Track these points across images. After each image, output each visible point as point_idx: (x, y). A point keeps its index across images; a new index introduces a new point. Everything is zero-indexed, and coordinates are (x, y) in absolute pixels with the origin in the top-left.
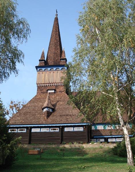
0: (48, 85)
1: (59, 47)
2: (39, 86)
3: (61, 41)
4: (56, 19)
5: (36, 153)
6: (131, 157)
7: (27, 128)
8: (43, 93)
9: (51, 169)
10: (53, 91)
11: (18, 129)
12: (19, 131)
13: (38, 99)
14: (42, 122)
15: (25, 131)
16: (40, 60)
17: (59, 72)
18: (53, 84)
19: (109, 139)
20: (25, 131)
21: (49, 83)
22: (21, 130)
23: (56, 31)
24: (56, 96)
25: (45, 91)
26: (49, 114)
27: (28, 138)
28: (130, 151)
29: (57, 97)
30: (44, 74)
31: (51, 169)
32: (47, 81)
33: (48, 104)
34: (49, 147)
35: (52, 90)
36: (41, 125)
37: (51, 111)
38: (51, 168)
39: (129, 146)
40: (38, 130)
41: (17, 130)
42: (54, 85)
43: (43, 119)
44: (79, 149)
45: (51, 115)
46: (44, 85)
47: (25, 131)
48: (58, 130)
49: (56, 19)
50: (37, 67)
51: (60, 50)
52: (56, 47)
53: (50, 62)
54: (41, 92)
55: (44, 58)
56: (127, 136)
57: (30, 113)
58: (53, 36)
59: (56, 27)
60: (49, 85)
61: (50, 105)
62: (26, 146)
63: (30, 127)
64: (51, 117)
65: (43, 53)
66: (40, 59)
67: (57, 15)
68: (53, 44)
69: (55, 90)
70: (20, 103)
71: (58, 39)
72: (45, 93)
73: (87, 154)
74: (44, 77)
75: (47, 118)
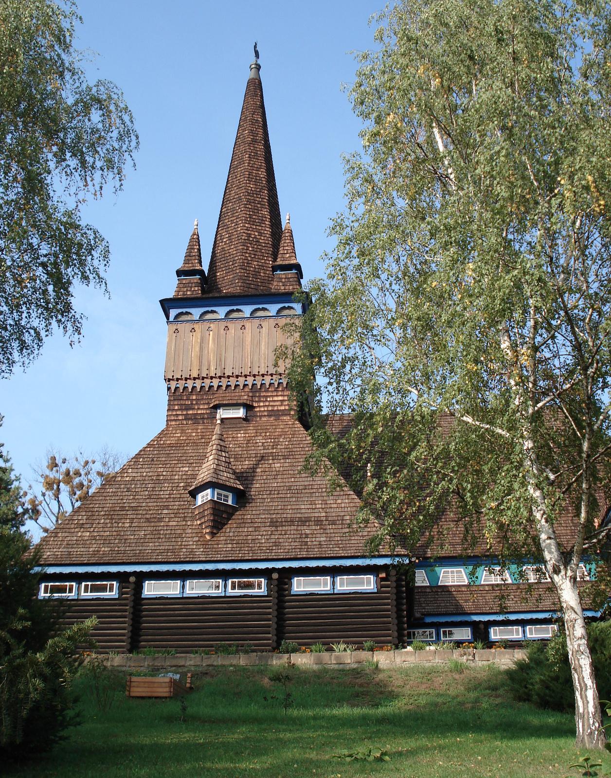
1: (266, 212)
2: (177, 388)
4: (255, 88)
6: (591, 709)
7: (121, 577)
8: (195, 419)
10: (240, 413)
16: (179, 273)
17: (265, 324)
18: (241, 381)
19: (492, 630)
20: (114, 594)
21: (220, 377)
22: (95, 589)
23: (254, 141)
28: (589, 682)
29: (260, 440)
30: (198, 335)
32: (212, 368)
35: (236, 405)
37: (230, 503)
39: (582, 662)
40: (171, 589)
41: (79, 589)
42: (245, 385)
43: (193, 536)
44: (356, 673)
45: (229, 519)
46: (198, 384)
48: (260, 588)
49: (255, 88)
51: (272, 226)
53: (228, 282)
55: (200, 263)
56: (573, 616)
57: (134, 509)
58: (241, 162)
59: (253, 122)
60: (219, 387)
61: (226, 477)
63: (135, 573)
64: (230, 529)
65: (195, 241)
66: (179, 264)
67: (258, 67)
69: (249, 407)
70: (90, 464)
71: (263, 174)
73: (392, 696)
74: (198, 349)
75: (213, 534)
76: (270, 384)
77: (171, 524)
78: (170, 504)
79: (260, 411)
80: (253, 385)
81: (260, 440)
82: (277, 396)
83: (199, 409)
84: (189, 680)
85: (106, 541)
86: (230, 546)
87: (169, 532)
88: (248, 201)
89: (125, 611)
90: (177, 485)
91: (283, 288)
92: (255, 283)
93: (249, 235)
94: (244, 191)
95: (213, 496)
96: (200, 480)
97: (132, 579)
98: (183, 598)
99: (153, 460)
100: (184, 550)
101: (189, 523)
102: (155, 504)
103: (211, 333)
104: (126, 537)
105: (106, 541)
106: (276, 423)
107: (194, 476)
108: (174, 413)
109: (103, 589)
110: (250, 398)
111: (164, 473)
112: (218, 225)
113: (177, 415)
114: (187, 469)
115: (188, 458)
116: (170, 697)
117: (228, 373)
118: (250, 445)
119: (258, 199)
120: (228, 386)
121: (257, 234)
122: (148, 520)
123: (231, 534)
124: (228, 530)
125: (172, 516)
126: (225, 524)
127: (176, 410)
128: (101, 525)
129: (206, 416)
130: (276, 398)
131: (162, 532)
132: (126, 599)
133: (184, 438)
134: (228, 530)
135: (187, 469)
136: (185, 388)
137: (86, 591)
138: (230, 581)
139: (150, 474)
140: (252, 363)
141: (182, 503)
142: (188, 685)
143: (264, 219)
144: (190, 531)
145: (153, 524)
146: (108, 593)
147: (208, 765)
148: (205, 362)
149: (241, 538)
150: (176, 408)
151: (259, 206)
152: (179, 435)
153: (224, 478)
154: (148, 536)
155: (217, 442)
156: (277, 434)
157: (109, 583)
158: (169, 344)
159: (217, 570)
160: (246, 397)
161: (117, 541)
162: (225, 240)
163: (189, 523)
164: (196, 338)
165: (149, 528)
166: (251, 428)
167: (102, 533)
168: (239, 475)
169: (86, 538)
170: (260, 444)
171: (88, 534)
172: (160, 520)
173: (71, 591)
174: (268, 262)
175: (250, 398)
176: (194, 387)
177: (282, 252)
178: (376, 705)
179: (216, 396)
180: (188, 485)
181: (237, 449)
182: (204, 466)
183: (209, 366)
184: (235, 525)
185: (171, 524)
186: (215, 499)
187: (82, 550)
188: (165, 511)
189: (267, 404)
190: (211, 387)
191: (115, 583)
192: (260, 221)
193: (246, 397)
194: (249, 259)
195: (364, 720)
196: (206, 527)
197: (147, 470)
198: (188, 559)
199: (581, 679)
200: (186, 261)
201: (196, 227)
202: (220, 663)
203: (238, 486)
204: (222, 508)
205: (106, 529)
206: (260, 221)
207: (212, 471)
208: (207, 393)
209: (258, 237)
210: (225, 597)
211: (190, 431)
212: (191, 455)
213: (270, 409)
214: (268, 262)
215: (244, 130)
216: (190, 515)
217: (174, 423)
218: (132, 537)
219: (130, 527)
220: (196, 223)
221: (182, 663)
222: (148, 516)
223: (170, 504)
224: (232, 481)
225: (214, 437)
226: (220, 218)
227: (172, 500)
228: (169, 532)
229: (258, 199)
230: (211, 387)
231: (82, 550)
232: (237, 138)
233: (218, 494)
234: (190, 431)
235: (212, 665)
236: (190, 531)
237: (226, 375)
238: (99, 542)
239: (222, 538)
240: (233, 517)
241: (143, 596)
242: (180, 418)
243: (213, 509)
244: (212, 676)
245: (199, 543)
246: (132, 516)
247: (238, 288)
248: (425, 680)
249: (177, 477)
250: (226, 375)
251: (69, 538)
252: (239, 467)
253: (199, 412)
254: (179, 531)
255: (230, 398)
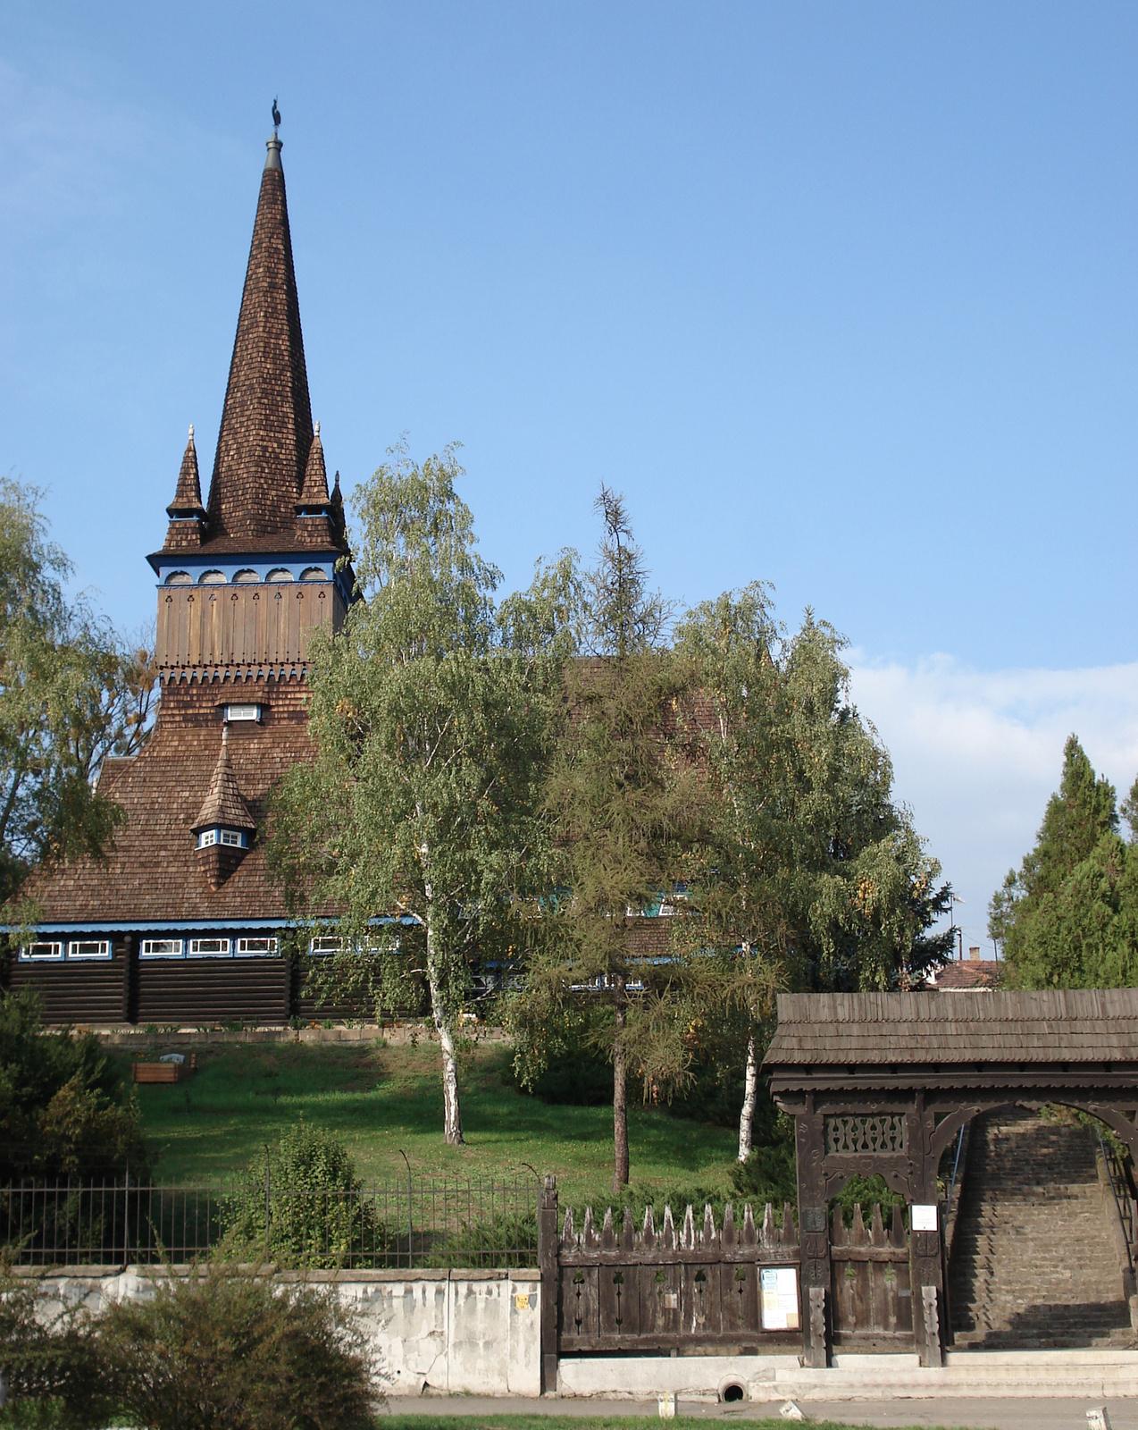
0: (221, 673)
1: (287, 409)
2: (172, 679)
3: (306, 387)
4: (274, 184)
5: (169, 1076)
6: (453, 1119)
7: (116, 937)
8: (197, 721)
9: (216, 1155)
10: (253, 714)
11: (66, 944)
12: (74, 952)
13: (166, 759)
14: (195, 907)
15: (105, 953)
16: (171, 512)
17: (284, 593)
18: (255, 670)
20: (107, 955)
21: (227, 666)
22: (84, 949)
23: (273, 286)
24: (268, 741)
25: (205, 709)
26: (227, 862)
27: (121, 974)
28: (453, 1100)
29: (277, 753)
30: (197, 604)
31: (216, 1155)
32: (217, 653)
33: (222, 809)
34: (228, 1043)
35: (249, 704)
36: (190, 926)
37: (239, 845)
38: (217, 1151)
39: (450, 1088)
40: (175, 950)
41: (66, 950)
42: (259, 677)
43: (196, 886)
44: (362, 1051)
45: (238, 864)
46: (199, 674)
47: (107, 955)
49: (274, 184)
50: (156, 561)
51: (296, 432)
52: (274, 408)
53: (239, 534)
54: (186, 719)
55: (199, 496)
56: (447, 1057)
58: (254, 324)
59: (272, 251)
60: (226, 678)
62: (110, 1033)
63: (130, 933)
64: (239, 879)
65: (191, 460)
67: (279, 146)
68: (251, 387)
69: (264, 707)
71: (284, 344)
72: (207, 720)
73: (384, 1076)
74: (197, 625)
75: (219, 885)
76: (292, 676)
77: (170, 870)
78: (168, 843)
79: (278, 712)
80: (270, 676)
81: (277, 753)
82: (300, 692)
83: (201, 707)
84: (193, 1061)
85: (95, 892)
86: (239, 899)
87: (167, 881)
88: (264, 391)
89: (121, 974)
90: (175, 816)
91: (308, 540)
92: (273, 524)
93: (265, 449)
94: (257, 375)
95: (219, 840)
96: (204, 817)
97: (128, 939)
98: (186, 959)
99: (145, 781)
100: (186, 905)
101: (191, 869)
102: (150, 843)
103: (215, 602)
104: (117, 887)
105: (95, 892)
106: (298, 729)
107: (198, 806)
108: (170, 712)
109: (94, 949)
110: (266, 695)
111: (160, 800)
112: (222, 426)
113: (173, 715)
114: (187, 794)
115: (189, 778)
116: (175, 1083)
117: (238, 660)
118: (264, 760)
119: (277, 388)
120: (237, 678)
121: (275, 445)
122: (143, 865)
123: (240, 884)
124: (237, 880)
125: (171, 859)
126: (233, 872)
127: (172, 709)
128: (86, 871)
129: (210, 717)
130: (298, 695)
131: (160, 881)
132: (121, 960)
133: (184, 748)
134: (237, 880)
135: (187, 794)
136: (183, 679)
137: (74, 952)
138: (239, 940)
139: (142, 801)
140: (268, 647)
141: (183, 842)
142: (193, 1066)
143: (286, 420)
144: (192, 880)
145: (148, 870)
146: (100, 954)
147: (202, 1155)
148: (208, 644)
149: (252, 889)
150: (172, 705)
151: (279, 399)
152: (176, 743)
153: (231, 817)
154: (144, 887)
155: (222, 770)
156: (298, 745)
157: (100, 943)
158: (160, 617)
159: (225, 929)
160: (260, 694)
161: (107, 892)
162: (232, 453)
163: (191, 869)
164: (194, 610)
165: (145, 876)
166: (267, 735)
167: (89, 882)
168: (251, 804)
169: (70, 888)
170: (278, 760)
171: (72, 882)
172: (157, 864)
173: (56, 952)
174: (290, 489)
175: (266, 695)
176: (194, 678)
177: (308, 484)
178: (372, 1088)
179: (222, 691)
180: (190, 818)
181: (249, 767)
182: (208, 799)
183: (213, 649)
184: (245, 873)
185: (170, 870)
186: (222, 843)
187: (67, 903)
188: (163, 853)
189: (287, 702)
190: (216, 678)
191: (107, 942)
192: (280, 424)
193: (260, 694)
194: (265, 486)
195: (344, 1108)
196: (211, 876)
197: (139, 795)
198: (190, 917)
199: (449, 1099)
200: (180, 494)
201: (191, 437)
202: (225, 1040)
203: (249, 825)
204: (230, 853)
205: (94, 876)
206: (280, 424)
207: (216, 808)
208: (210, 686)
209: (278, 450)
210: (234, 958)
211: (190, 738)
212: (192, 773)
213: (291, 709)
214: (290, 489)
215: (258, 267)
216: (192, 858)
217: (169, 725)
218: (125, 887)
219: (122, 873)
220: (191, 431)
221: (186, 1041)
222: (142, 860)
223: (168, 843)
224: (241, 818)
225: (219, 763)
226: (223, 416)
227: (170, 837)
228: (167, 881)
229: (277, 388)
230: (216, 678)
231: (67, 903)
232: (248, 278)
233: (225, 835)
234: (190, 738)
235: (217, 1043)
236: (192, 880)
237: (235, 663)
238: (86, 893)
239: (229, 890)
240: (244, 862)
241: (140, 958)
242: (177, 719)
243: (219, 854)
244: (217, 1055)
245: (203, 895)
246: (122, 860)
247: (250, 533)
248: (428, 1061)
249: (175, 806)
250: (235, 663)
251: (50, 888)
252: (252, 792)
253: (202, 711)
254: (180, 880)
255: (239, 694)
